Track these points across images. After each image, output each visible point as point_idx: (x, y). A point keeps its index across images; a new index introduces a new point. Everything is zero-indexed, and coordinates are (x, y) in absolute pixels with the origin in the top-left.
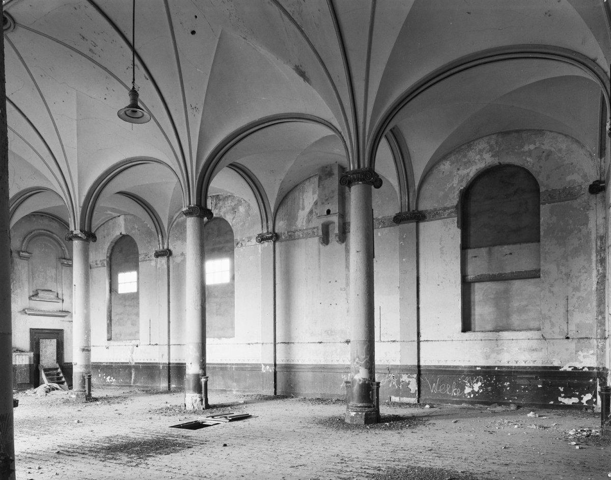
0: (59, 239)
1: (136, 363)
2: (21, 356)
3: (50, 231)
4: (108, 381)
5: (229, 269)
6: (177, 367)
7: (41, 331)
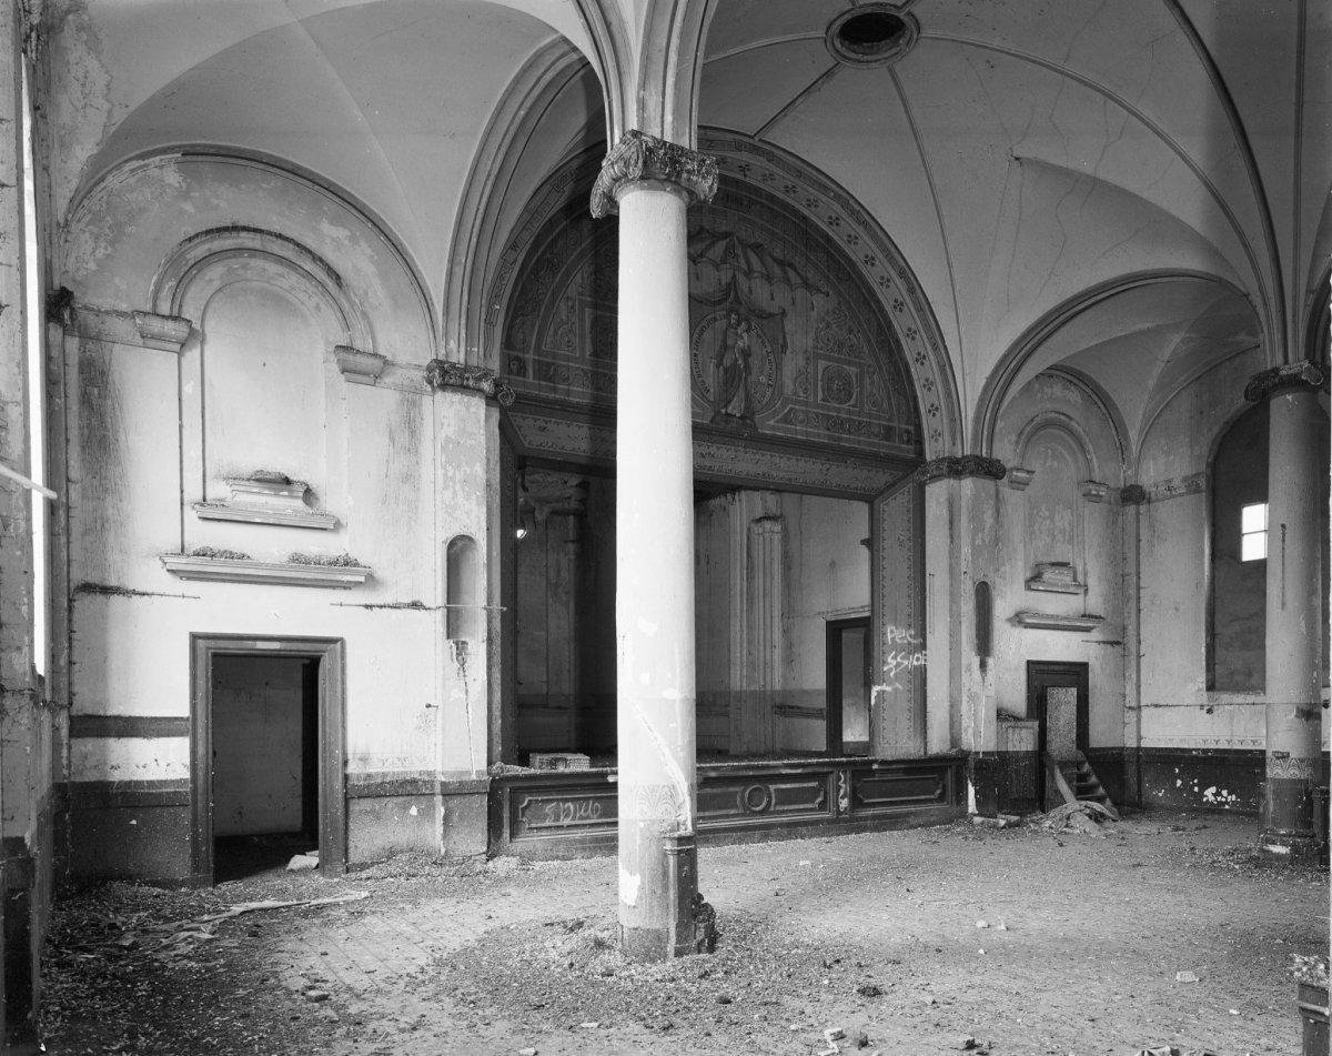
0: (1082, 433)
2: (1017, 731)
4: (1211, 798)
7: (1046, 668)
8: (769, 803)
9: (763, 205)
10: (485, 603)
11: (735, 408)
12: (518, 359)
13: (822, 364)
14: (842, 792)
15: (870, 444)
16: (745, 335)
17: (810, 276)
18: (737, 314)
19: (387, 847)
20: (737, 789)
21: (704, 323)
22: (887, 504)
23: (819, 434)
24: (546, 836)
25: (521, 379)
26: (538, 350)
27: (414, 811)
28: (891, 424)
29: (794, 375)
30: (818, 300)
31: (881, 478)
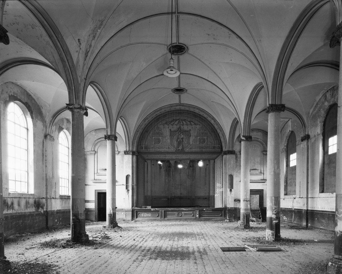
1: (294, 209)
3: (256, 138)
5: (9, 157)
6: (311, 212)
8: (182, 215)
11: (180, 148)
13: (198, 138)
14: (197, 214)
16: (182, 136)
18: (181, 132)
23: (198, 150)
24: (142, 218)
26: (145, 145)
27: (123, 213)
30: (198, 126)
31: (214, 156)
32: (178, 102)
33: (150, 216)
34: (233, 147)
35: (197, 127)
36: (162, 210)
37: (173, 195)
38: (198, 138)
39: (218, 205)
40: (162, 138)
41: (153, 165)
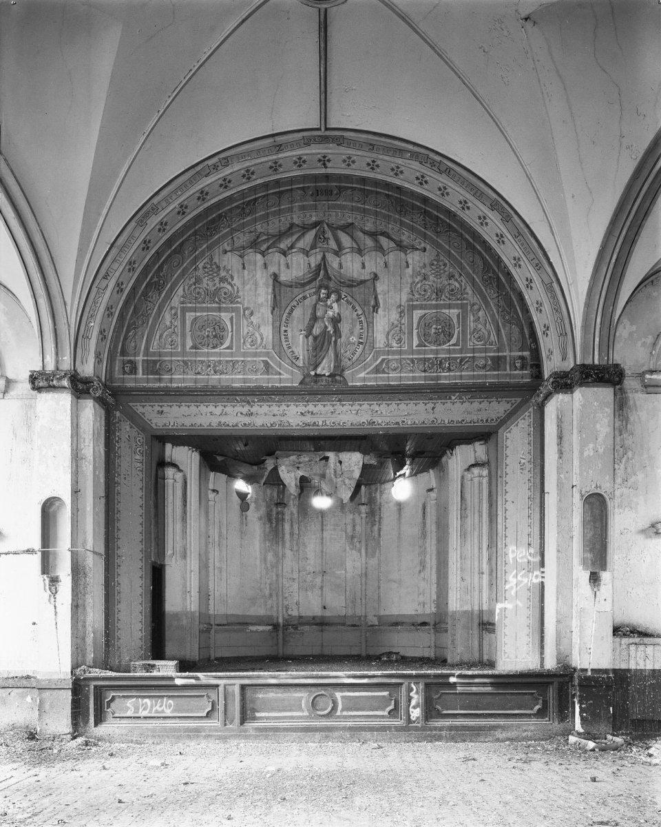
2: (641, 648)
8: (334, 708)
9: (353, 189)
10: (70, 546)
11: (325, 368)
12: (130, 362)
13: (417, 314)
14: (413, 703)
15: (474, 377)
16: (335, 305)
17: (404, 238)
18: (327, 288)
19: (11, 723)
20: (302, 695)
21: (294, 303)
22: (510, 432)
25: (133, 376)
26: (147, 353)
28: (500, 354)
29: (387, 330)
30: (414, 258)
31: (495, 409)
32: (313, 121)
33: (168, 713)
34: (608, 341)
35: (410, 261)
36: (230, 682)
37: (295, 613)
38: (417, 314)
39: (515, 654)
40: (231, 319)
41: (214, 491)
